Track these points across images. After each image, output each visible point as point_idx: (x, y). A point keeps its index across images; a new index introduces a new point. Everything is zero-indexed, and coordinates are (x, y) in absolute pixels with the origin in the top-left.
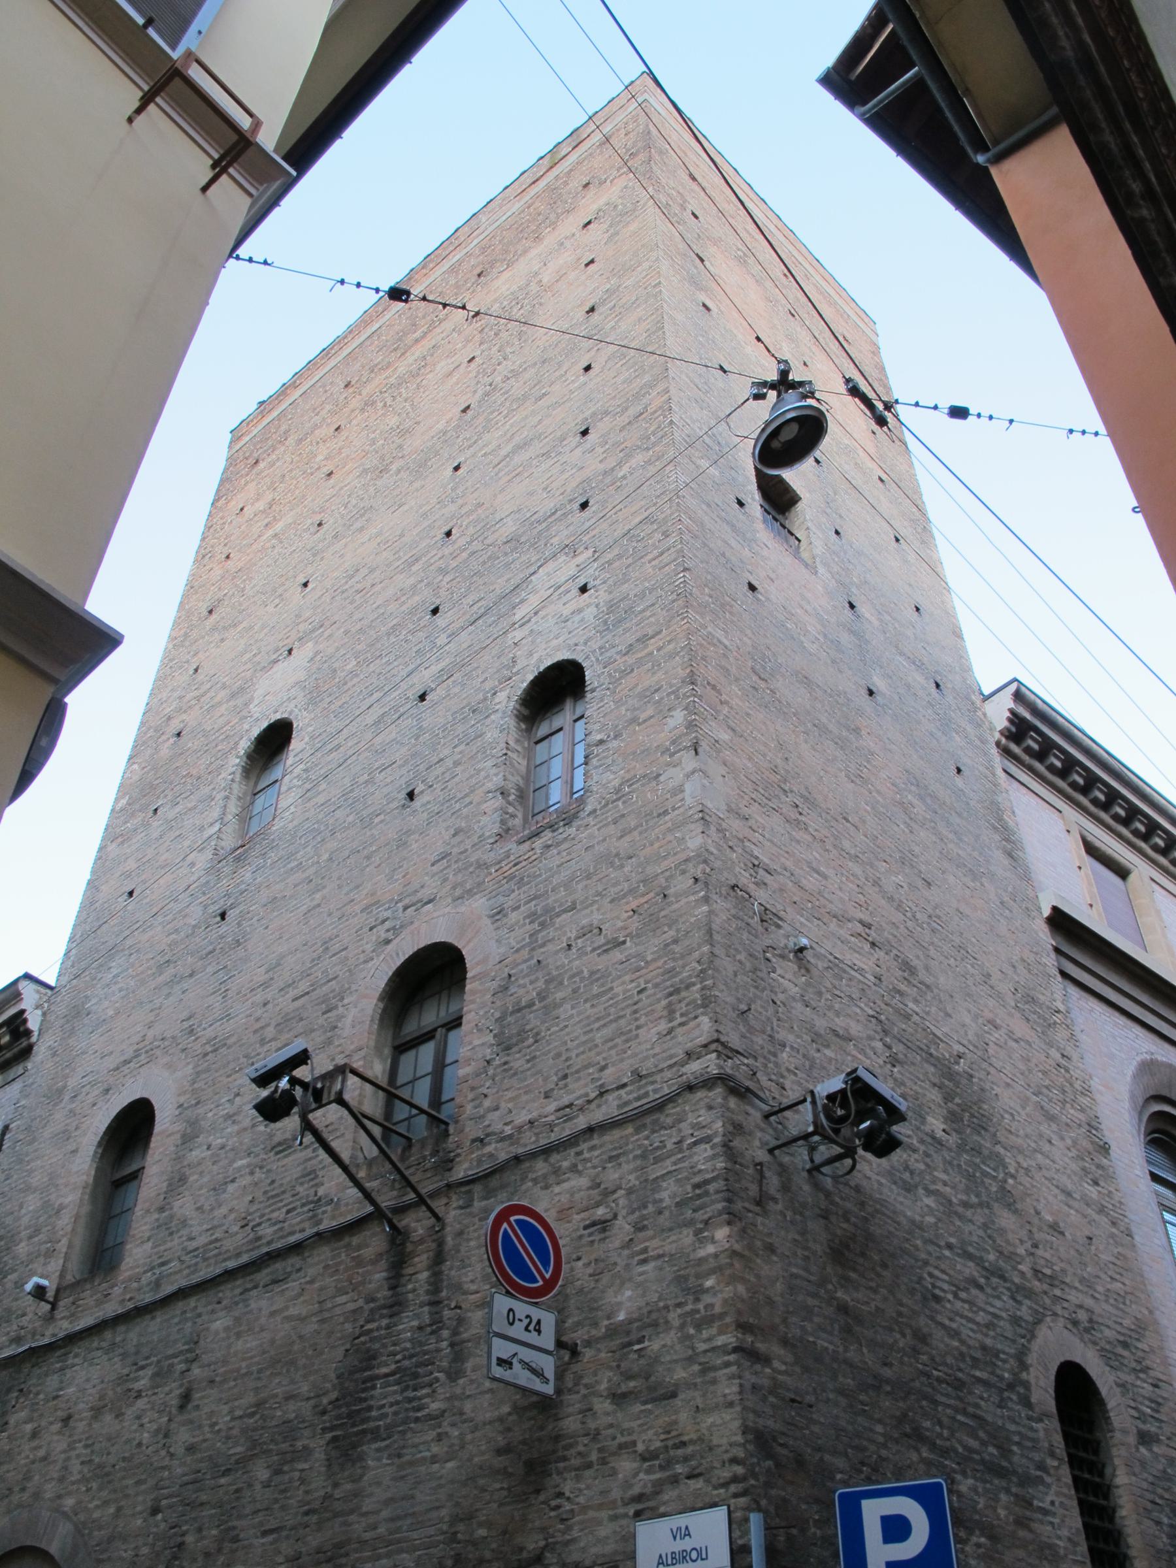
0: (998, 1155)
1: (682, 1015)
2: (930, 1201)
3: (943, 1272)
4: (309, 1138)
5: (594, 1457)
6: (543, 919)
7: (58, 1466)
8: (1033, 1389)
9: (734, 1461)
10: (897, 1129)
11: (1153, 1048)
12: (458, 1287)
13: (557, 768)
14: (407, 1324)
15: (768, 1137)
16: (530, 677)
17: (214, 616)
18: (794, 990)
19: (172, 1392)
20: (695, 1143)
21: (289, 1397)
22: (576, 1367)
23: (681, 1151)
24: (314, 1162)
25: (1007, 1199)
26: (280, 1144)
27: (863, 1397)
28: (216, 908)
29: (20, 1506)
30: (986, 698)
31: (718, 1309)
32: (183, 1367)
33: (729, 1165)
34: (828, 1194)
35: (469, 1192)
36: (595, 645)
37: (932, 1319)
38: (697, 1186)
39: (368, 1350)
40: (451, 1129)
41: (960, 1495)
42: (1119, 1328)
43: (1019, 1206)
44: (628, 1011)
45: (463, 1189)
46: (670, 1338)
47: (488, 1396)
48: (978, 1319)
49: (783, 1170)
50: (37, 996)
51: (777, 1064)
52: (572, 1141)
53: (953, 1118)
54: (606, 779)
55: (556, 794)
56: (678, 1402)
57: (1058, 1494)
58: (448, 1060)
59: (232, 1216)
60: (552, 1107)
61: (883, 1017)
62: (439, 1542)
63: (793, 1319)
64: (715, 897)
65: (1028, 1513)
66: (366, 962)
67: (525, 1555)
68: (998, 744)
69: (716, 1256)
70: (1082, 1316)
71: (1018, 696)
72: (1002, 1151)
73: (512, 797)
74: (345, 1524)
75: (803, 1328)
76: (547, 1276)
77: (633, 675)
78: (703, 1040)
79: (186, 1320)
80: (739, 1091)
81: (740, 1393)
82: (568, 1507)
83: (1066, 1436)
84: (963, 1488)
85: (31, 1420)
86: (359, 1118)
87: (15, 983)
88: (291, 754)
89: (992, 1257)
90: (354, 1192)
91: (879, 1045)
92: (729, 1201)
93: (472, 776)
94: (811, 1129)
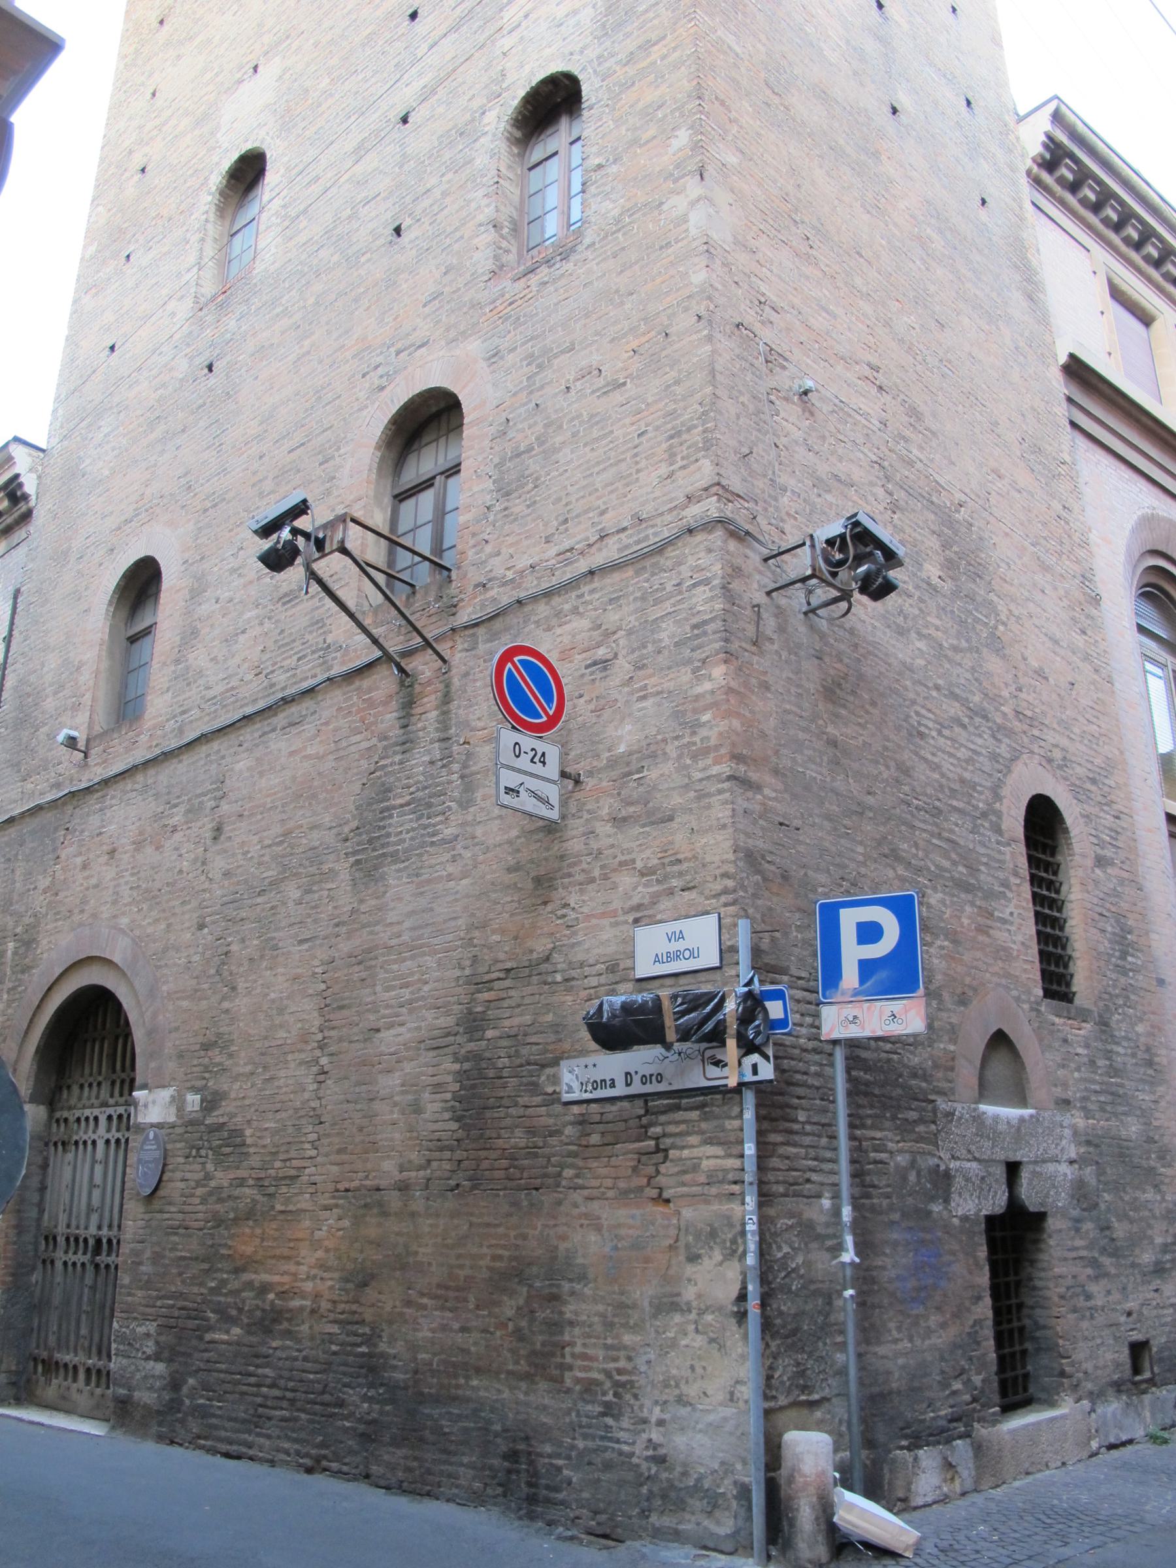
0: (991, 602)
1: (683, 458)
2: (921, 645)
3: (929, 711)
4: (315, 587)
5: (597, 873)
6: (539, 361)
7: (111, 891)
8: (1005, 817)
9: (725, 875)
10: (893, 574)
11: (1156, 503)
12: (466, 724)
13: (552, 197)
14: (419, 759)
15: (766, 580)
16: (522, 93)
17: (166, 27)
18: (798, 435)
19: (205, 827)
20: (694, 585)
21: (313, 827)
22: (577, 795)
23: (680, 593)
24: (321, 611)
25: (996, 645)
26: (286, 595)
27: (846, 822)
28: (203, 360)
29: (81, 925)
30: (1021, 119)
31: (713, 742)
32: (213, 803)
33: (727, 606)
34: (822, 636)
35: (474, 635)
36: (591, 54)
37: (917, 754)
38: (695, 627)
39: (383, 784)
40: (454, 575)
41: (929, 906)
42: (1089, 766)
43: (1007, 652)
44: (629, 455)
45: (467, 632)
46: (668, 767)
47: (497, 822)
48: (959, 755)
49: (780, 612)
50: (29, 460)
51: (777, 509)
52: (572, 584)
53: (950, 565)
54: (606, 208)
55: (552, 226)
56: (674, 825)
57: (1017, 907)
58: (449, 508)
59: (246, 665)
60: (553, 551)
61: (886, 464)
62: (457, 947)
63: (784, 751)
64: (719, 336)
65: (989, 922)
66: (360, 410)
67: (535, 955)
68: (1029, 173)
69: (713, 692)
70: (1057, 754)
71: (1057, 117)
72: (995, 599)
73: (505, 231)
74: (371, 933)
75: (794, 760)
76: (551, 713)
77: (634, 88)
78: (704, 483)
79: (211, 762)
80: (740, 535)
81: (733, 816)
82: (573, 915)
83: (1030, 858)
84: (933, 901)
85: (80, 854)
86: (363, 567)
87: (7, 445)
88: (267, 189)
89: (977, 699)
90: (362, 638)
91: (880, 492)
92: (727, 640)
93: (462, 208)
94: (809, 572)
